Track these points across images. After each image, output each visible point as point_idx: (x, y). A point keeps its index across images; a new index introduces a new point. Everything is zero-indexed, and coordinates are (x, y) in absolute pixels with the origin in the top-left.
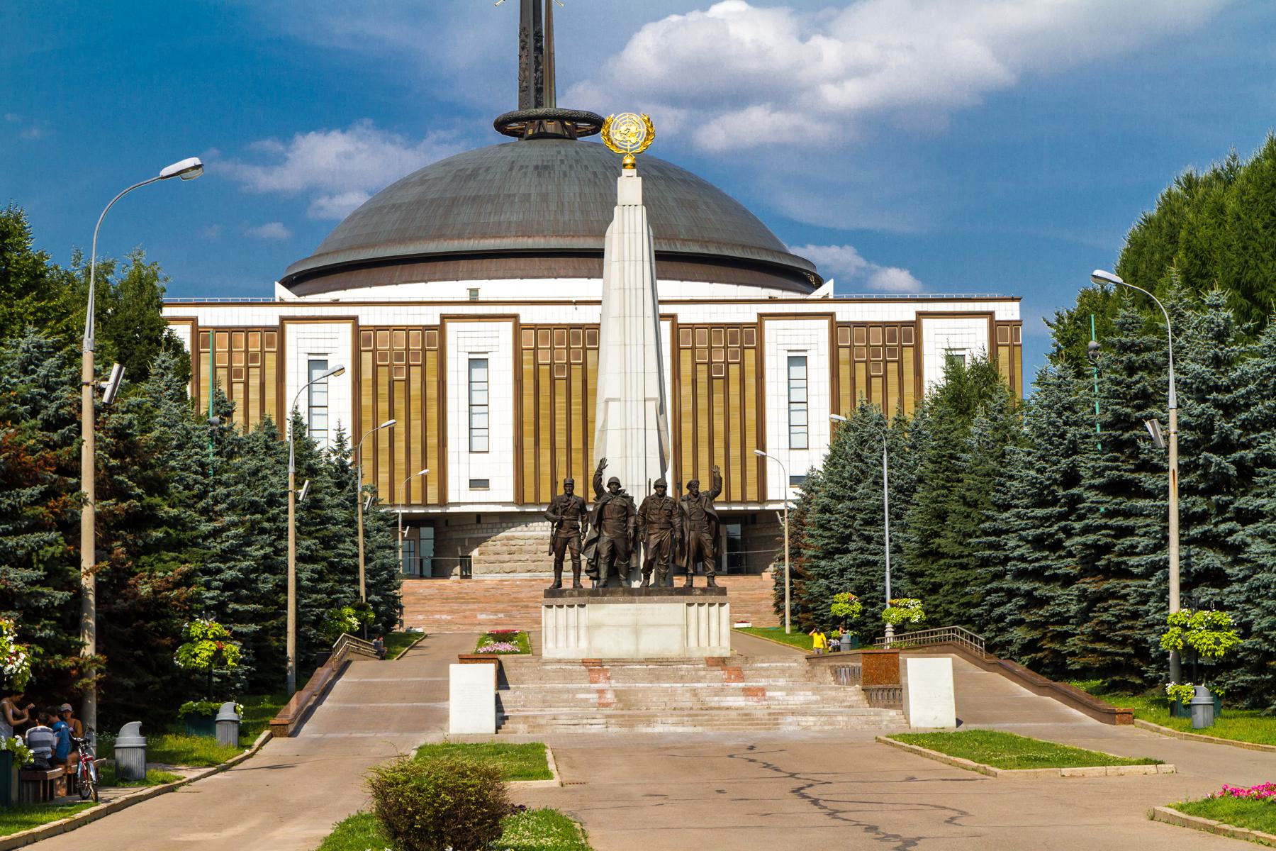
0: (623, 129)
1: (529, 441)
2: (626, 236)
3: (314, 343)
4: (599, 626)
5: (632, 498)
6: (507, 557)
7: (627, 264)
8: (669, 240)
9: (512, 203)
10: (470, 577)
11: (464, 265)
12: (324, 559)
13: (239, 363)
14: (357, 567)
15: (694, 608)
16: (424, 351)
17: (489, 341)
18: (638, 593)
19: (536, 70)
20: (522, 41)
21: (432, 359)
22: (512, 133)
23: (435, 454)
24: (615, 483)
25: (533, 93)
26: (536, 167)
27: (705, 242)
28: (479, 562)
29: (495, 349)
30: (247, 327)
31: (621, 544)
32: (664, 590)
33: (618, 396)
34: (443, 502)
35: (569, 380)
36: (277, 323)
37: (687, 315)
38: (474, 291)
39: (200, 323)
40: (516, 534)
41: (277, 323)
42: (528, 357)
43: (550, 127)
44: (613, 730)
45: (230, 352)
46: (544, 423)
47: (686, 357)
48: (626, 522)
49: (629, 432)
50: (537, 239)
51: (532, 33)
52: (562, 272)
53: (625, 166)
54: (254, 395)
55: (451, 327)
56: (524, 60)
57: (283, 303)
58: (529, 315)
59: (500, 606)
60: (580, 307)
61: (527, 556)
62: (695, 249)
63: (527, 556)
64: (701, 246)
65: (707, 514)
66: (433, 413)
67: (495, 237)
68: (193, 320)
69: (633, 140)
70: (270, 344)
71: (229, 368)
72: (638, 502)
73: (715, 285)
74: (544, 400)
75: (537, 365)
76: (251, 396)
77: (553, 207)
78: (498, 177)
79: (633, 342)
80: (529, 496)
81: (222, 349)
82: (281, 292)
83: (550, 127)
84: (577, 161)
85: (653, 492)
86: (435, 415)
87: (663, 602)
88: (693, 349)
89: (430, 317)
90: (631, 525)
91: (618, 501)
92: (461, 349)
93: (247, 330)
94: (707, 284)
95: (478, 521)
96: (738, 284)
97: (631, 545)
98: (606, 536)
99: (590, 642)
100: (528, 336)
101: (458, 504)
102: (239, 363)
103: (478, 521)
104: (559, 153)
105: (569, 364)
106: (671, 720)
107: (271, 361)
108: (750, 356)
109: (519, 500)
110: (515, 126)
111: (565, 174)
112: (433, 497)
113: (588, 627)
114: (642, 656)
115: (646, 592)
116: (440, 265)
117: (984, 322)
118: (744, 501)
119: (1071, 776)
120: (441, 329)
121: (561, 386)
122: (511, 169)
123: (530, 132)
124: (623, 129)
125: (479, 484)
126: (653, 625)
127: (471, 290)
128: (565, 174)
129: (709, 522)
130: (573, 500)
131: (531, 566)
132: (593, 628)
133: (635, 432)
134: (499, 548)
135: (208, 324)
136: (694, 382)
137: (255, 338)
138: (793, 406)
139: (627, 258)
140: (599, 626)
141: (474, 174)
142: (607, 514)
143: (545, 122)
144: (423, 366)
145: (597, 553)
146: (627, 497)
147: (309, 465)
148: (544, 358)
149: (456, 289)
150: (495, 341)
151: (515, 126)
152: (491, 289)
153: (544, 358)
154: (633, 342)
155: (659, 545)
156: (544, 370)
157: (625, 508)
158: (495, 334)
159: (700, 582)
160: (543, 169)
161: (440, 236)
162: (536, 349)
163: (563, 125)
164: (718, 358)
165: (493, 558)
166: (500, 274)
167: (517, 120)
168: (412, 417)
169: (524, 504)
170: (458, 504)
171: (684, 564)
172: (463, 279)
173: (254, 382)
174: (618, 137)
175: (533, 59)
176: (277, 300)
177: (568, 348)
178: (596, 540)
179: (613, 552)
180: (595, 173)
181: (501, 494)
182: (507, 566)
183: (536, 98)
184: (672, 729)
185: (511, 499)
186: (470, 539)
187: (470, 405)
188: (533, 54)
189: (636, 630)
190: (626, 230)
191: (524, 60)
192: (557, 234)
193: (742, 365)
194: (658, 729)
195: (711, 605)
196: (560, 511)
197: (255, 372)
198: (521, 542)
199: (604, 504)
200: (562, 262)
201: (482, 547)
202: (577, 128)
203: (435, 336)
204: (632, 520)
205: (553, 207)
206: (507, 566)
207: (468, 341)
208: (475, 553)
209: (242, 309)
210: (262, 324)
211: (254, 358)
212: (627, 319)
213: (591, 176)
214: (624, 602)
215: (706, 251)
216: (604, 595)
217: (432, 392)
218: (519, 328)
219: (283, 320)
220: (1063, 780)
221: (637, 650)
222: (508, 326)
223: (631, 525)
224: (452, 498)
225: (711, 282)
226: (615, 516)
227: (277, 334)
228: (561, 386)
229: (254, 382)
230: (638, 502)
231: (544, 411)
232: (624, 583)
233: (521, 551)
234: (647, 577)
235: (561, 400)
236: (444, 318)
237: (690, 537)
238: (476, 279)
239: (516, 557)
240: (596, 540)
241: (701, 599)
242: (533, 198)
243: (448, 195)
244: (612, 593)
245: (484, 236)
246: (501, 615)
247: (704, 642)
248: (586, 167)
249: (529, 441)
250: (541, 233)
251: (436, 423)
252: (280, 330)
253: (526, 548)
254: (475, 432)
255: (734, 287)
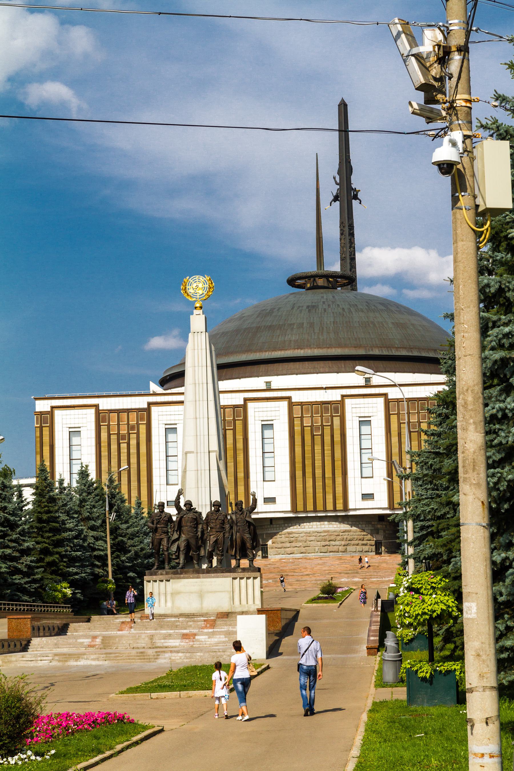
0: (194, 285)
1: (299, 473)
2: (196, 351)
3: (169, 417)
4: (178, 593)
5: (201, 513)
6: (288, 545)
7: (196, 368)
8: (387, 348)
9: (292, 329)
10: (267, 557)
11: (263, 367)
12: (57, 553)
13: (124, 431)
14: (106, 555)
15: (237, 581)
16: (235, 420)
17: (273, 413)
18: (204, 572)
19: (350, 247)
20: (341, 230)
21: (239, 425)
22: (299, 287)
23: (243, 483)
24: (189, 504)
25: (348, 261)
26: (308, 307)
27: (411, 349)
28: (272, 548)
29: (277, 418)
30: (128, 410)
31: (193, 542)
32: (225, 568)
33: (193, 450)
34: (346, 508)
35: (322, 435)
36: (146, 406)
37: (394, 393)
38: (268, 383)
39: (101, 408)
40: (294, 530)
41: (146, 406)
42: (297, 422)
43: (320, 282)
44: (54, 663)
45: (118, 425)
46: (308, 462)
47: (394, 419)
48: (197, 528)
49: (199, 472)
50: (306, 350)
51: (347, 225)
52: (321, 370)
53: (196, 308)
54: (133, 450)
55: (251, 405)
56: (343, 241)
57: (155, 394)
58: (297, 397)
59: (271, 575)
60: (328, 391)
61: (301, 544)
62: (404, 353)
63: (301, 544)
64: (408, 351)
65: (247, 522)
66: (240, 458)
67: (281, 350)
68: (96, 406)
69: (201, 292)
70: (142, 419)
71: (118, 434)
72: (204, 516)
73: (416, 374)
74: (308, 448)
75: (303, 427)
76: (131, 451)
77: (317, 331)
78: (284, 314)
79: (201, 416)
80: (300, 507)
81: (114, 423)
82: (154, 387)
83: (320, 282)
84: (333, 302)
85: (213, 508)
86: (242, 459)
87: (218, 577)
88: (398, 414)
89: (335, 396)
90: (200, 530)
91: (191, 515)
92: (257, 418)
93: (128, 411)
94: (411, 374)
95: (271, 523)
96: (431, 373)
97: (200, 542)
98: (183, 537)
99: (173, 603)
100: (297, 410)
101: (355, 510)
102: (124, 431)
103: (271, 523)
104: (323, 297)
105: (322, 426)
106: (92, 657)
107: (143, 429)
108: (337, 421)
109: (294, 509)
110: (299, 282)
111: (325, 310)
112: (340, 506)
113: (172, 594)
114: (176, 612)
115: (210, 570)
116: (249, 368)
117: (381, 400)
118: (335, 510)
119: (157, 698)
120: (244, 407)
121: (318, 439)
122: (293, 308)
123: (309, 285)
124: (194, 285)
125: (367, 496)
126: (211, 592)
127: (267, 382)
128: (325, 310)
129: (249, 527)
130: (163, 515)
131: (303, 550)
132: (174, 594)
133: (203, 471)
134: (283, 539)
135: (105, 408)
136: (400, 435)
137: (133, 416)
138: (363, 451)
139: (196, 365)
140: (178, 593)
141: (272, 311)
142: (183, 523)
143: (317, 279)
144: (234, 430)
145: (178, 548)
146: (196, 512)
147: (50, 496)
148: (307, 422)
149: (257, 382)
150: (277, 413)
151: (299, 282)
152: (279, 381)
153: (307, 422)
154: (201, 416)
155: (216, 542)
156: (308, 430)
157: (196, 519)
158: (277, 409)
159: (245, 563)
160: (311, 308)
161: (248, 351)
162: (302, 418)
163: (328, 281)
164: (414, 419)
165: (280, 545)
166: (285, 372)
167: (300, 278)
168: (228, 460)
169: (307, 512)
170: (355, 510)
171: (233, 553)
172: (261, 376)
173: (133, 442)
174: (191, 291)
175: (348, 241)
176: (152, 392)
177: (322, 416)
178: (178, 539)
179: (188, 547)
180: (343, 309)
181: (283, 506)
182: (289, 550)
183: (351, 264)
184: (94, 663)
185: (289, 508)
186: (266, 534)
187: (263, 453)
188: (348, 238)
189: (201, 595)
190: (196, 348)
191: (343, 241)
192: (319, 347)
193: (332, 426)
194: (82, 663)
195: (248, 578)
196: (155, 522)
197: (133, 436)
198: (297, 535)
199: (182, 517)
200: (321, 363)
201: (274, 539)
202: (337, 282)
203: (337, 408)
204: (200, 526)
205: (317, 331)
206: (289, 550)
207: (261, 414)
208: (270, 543)
209: (121, 399)
210: (137, 407)
211: (133, 428)
212: (197, 402)
213: (341, 311)
214: (193, 578)
215: (410, 354)
216: (181, 573)
217: (240, 445)
218: (291, 405)
219: (150, 404)
220: (152, 700)
221: (202, 608)
222: (284, 404)
223: (200, 530)
224: (351, 506)
225: (414, 373)
226: (188, 524)
227: (146, 413)
228: (318, 439)
229: (133, 442)
230: (204, 516)
231: (308, 455)
232: (196, 566)
233: (297, 541)
234: (211, 562)
235: (318, 448)
236: (246, 400)
237: (237, 536)
238: (269, 376)
239: (294, 544)
240: (178, 539)
241: (241, 575)
242: (305, 325)
243: (254, 325)
244: (186, 573)
245: (275, 349)
246: (270, 581)
247: (244, 602)
248: (338, 305)
249: (299, 473)
250: (309, 347)
251: (242, 464)
252: (148, 410)
253: (300, 539)
254: (266, 469)
255: (428, 375)
